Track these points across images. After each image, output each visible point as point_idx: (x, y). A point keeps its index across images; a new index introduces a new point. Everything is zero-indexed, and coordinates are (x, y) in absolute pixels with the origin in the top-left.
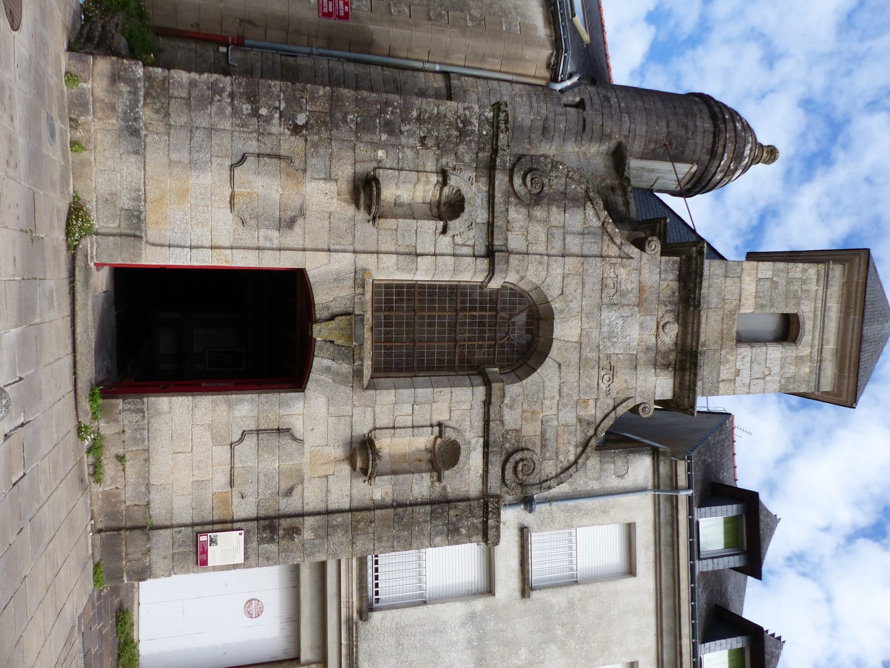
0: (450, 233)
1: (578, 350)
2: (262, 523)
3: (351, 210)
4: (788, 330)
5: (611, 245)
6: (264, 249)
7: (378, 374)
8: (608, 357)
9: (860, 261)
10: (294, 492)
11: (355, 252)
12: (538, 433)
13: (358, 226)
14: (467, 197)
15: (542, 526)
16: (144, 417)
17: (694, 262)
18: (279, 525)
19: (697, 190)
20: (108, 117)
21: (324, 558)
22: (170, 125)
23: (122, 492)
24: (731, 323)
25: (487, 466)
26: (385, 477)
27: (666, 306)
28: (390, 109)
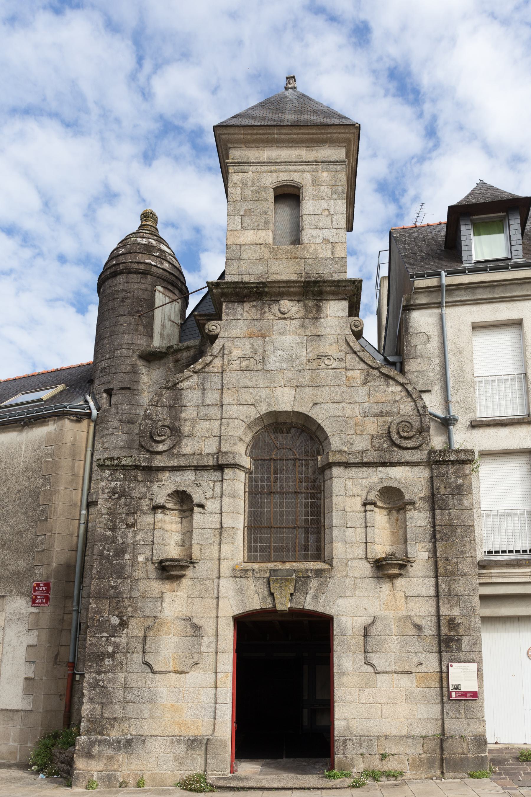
0: (203, 501)
1: (302, 388)
2: (443, 649)
3: (185, 581)
4: (288, 196)
5: (213, 364)
6: (217, 648)
7: (322, 556)
8: (309, 361)
9: (224, 134)
10: (419, 623)
11: (219, 578)
12: (375, 419)
13: (198, 575)
14: (173, 489)
15: (471, 408)
16: (349, 739)
17: (226, 290)
18: (446, 635)
19: (179, 284)
20: (118, 761)
21: (477, 598)
22: (123, 717)
23: (411, 756)
24: (281, 251)
25: (403, 463)
26: (409, 549)
27: (265, 312)
28: (105, 552)
